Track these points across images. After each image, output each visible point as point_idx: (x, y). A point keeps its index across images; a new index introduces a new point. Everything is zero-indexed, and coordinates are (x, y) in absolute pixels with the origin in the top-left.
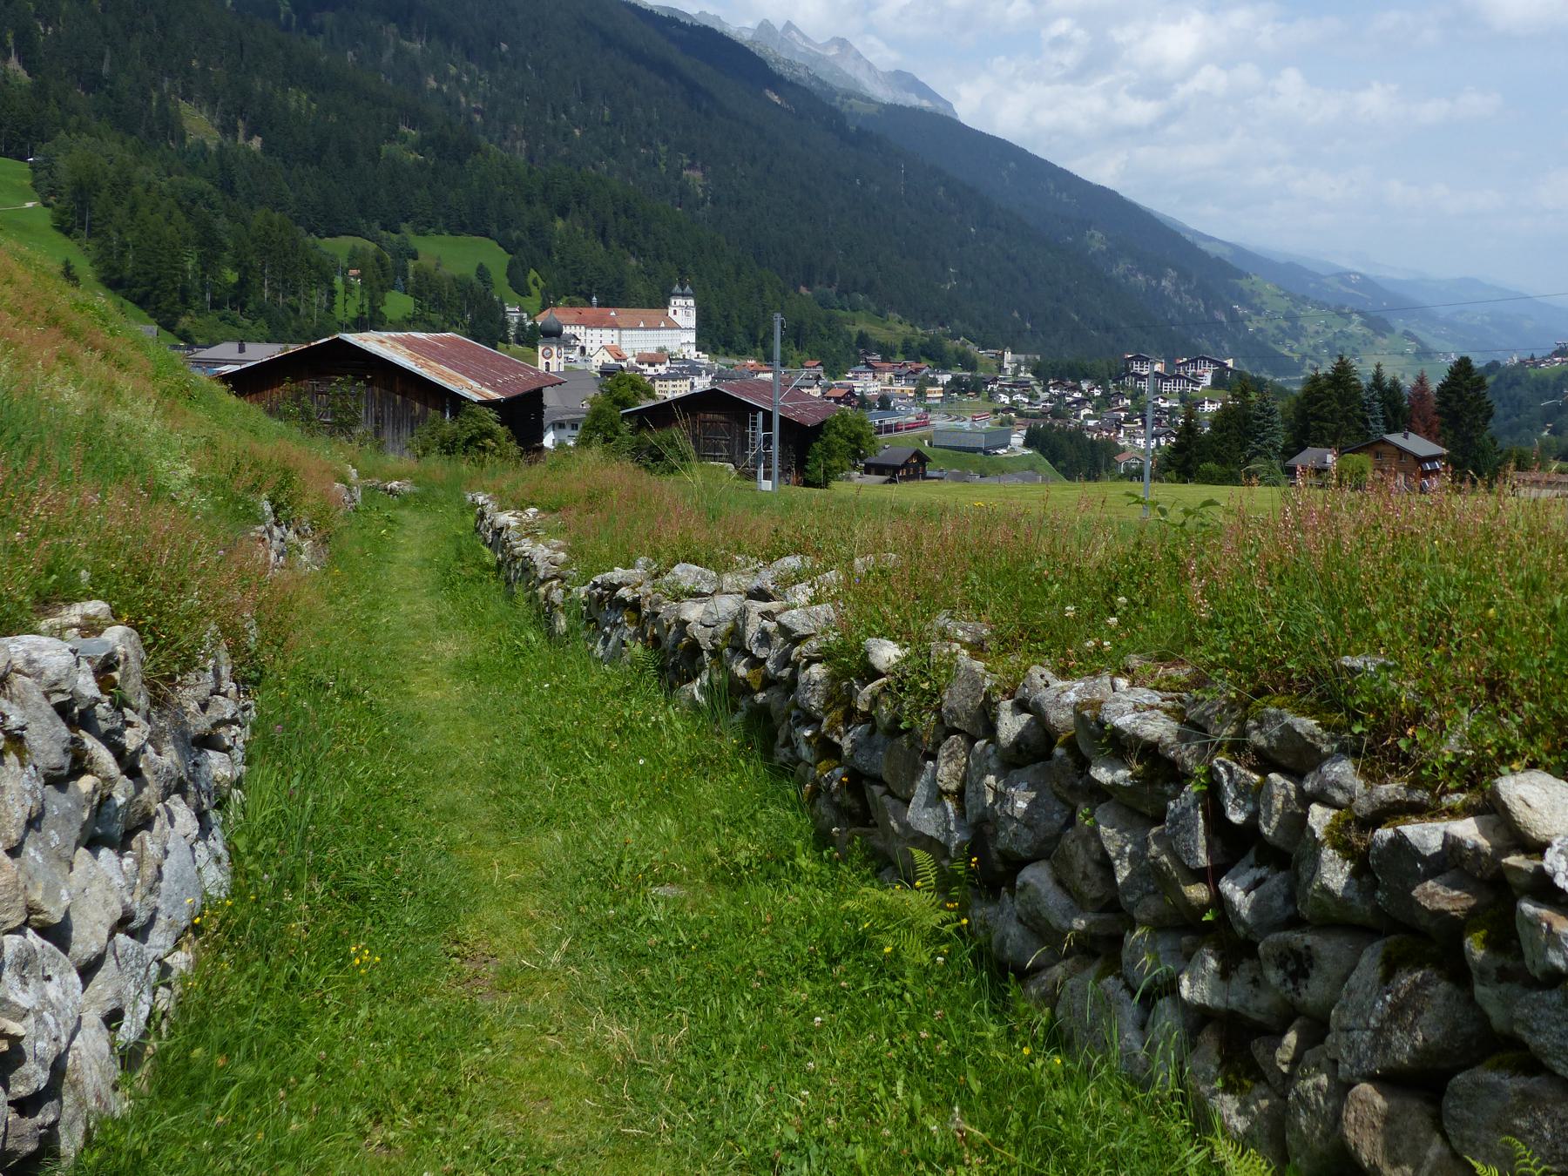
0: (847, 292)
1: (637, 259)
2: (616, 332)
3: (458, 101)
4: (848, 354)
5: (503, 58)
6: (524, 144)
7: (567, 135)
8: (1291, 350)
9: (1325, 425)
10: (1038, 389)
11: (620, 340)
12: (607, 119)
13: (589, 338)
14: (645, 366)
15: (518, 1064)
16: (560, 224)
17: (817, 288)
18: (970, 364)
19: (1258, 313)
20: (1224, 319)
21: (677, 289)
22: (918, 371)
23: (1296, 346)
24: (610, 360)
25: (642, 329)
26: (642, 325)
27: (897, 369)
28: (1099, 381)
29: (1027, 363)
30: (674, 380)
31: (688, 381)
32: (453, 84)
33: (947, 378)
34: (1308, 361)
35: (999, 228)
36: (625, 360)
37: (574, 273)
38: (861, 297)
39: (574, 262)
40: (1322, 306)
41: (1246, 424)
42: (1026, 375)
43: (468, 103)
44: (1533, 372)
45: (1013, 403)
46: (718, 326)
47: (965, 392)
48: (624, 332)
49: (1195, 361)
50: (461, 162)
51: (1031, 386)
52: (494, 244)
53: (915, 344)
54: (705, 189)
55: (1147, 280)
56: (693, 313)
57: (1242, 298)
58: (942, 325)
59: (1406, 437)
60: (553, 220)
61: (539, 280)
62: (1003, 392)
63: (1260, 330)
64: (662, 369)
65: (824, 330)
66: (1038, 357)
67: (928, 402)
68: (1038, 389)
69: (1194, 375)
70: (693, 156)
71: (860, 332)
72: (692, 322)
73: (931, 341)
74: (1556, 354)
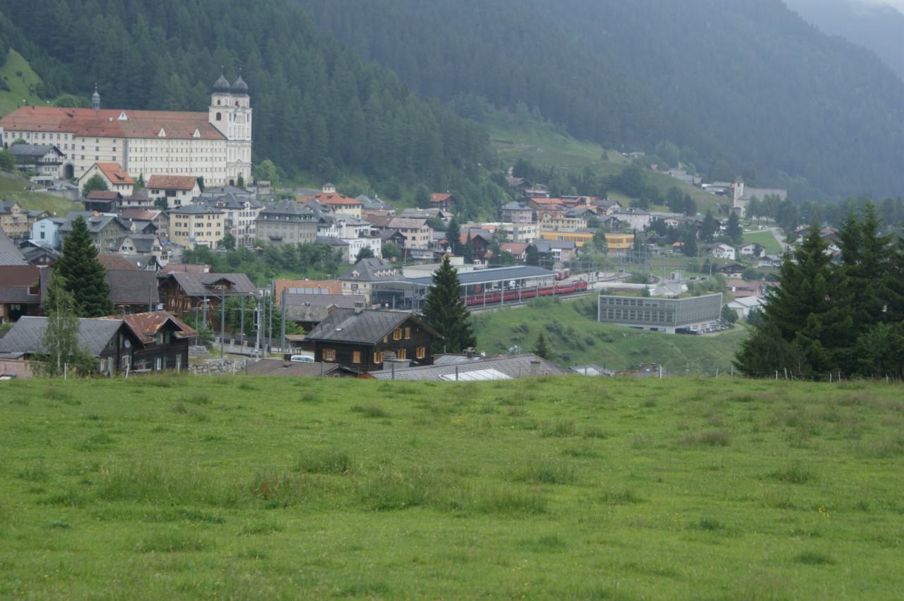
13: (78, 152)
15: (835, 302)
30: (199, 216)
33: (640, 222)
48: (133, 144)
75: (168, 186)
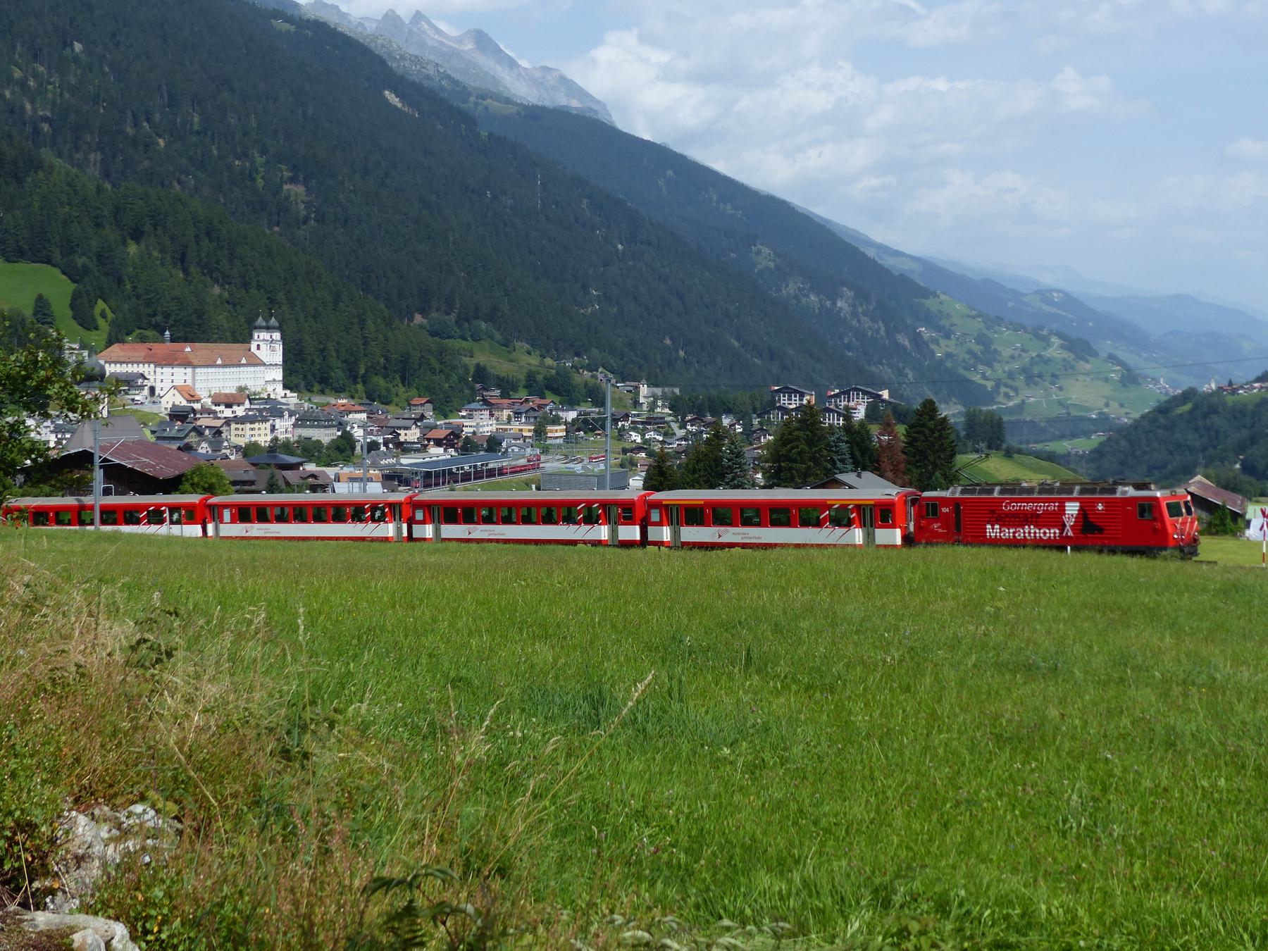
0: (467, 320)
1: (222, 286)
2: (189, 370)
3: (23, 108)
4: (462, 390)
5: (76, 59)
6: (99, 156)
7: (149, 146)
8: (984, 377)
9: (794, 465)
10: (675, 426)
11: (194, 379)
12: (196, 127)
13: (159, 377)
14: (222, 408)
16: (133, 249)
17: (434, 315)
18: (597, 397)
19: (948, 337)
20: (907, 343)
21: (260, 321)
22: (541, 407)
23: (989, 373)
24: (182, 402)
25: (219, 366)
26: (219, 362)
27: (517, 406)
28: (742, 416)
29: (664, 398)
30: (237, 423)
31: (268, 425)
32: (17, 89)
33: (571, 415)
34: (1003, 389)
35: (650, 244)
36: (198, 401)
37: (148, 303)
38: (483, 325)
39: (148, 292)
40: (1017, 327)
41: (717, 466)
42: (663, 410)
43: (34, 110)
44: (1230, 400)
45: (645, 441)
46: (313, 362)
47: (593, 430)
48: (198, 370)
49: (847, 393)
50: (19, 180)
51: (668, 423)
52: (57, 271)
53: (540, 378)
54: (308, 205)
55: (820, 301)
56: (279, 348)
57: (929, 319)
58: (578, 355)
59: (859, 476)
60: (125, 244)
61: (108, 312)
62: (635, 429)
63: (949, 355)
64: (240, 411)
65: (435, 363)
66: (677, 391)
67: (549, 442)
68: (675, 426)
69: (847, 408)
70: (294, 168)
71: (478, 366)
72: (278, 358)
73: (558, 373)
74: (1258, 380)
75: (226, 401)
